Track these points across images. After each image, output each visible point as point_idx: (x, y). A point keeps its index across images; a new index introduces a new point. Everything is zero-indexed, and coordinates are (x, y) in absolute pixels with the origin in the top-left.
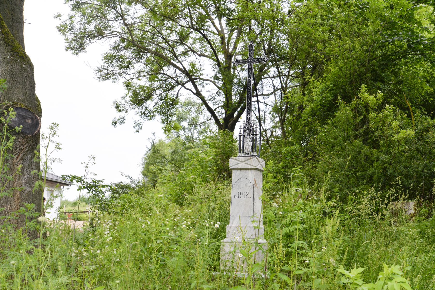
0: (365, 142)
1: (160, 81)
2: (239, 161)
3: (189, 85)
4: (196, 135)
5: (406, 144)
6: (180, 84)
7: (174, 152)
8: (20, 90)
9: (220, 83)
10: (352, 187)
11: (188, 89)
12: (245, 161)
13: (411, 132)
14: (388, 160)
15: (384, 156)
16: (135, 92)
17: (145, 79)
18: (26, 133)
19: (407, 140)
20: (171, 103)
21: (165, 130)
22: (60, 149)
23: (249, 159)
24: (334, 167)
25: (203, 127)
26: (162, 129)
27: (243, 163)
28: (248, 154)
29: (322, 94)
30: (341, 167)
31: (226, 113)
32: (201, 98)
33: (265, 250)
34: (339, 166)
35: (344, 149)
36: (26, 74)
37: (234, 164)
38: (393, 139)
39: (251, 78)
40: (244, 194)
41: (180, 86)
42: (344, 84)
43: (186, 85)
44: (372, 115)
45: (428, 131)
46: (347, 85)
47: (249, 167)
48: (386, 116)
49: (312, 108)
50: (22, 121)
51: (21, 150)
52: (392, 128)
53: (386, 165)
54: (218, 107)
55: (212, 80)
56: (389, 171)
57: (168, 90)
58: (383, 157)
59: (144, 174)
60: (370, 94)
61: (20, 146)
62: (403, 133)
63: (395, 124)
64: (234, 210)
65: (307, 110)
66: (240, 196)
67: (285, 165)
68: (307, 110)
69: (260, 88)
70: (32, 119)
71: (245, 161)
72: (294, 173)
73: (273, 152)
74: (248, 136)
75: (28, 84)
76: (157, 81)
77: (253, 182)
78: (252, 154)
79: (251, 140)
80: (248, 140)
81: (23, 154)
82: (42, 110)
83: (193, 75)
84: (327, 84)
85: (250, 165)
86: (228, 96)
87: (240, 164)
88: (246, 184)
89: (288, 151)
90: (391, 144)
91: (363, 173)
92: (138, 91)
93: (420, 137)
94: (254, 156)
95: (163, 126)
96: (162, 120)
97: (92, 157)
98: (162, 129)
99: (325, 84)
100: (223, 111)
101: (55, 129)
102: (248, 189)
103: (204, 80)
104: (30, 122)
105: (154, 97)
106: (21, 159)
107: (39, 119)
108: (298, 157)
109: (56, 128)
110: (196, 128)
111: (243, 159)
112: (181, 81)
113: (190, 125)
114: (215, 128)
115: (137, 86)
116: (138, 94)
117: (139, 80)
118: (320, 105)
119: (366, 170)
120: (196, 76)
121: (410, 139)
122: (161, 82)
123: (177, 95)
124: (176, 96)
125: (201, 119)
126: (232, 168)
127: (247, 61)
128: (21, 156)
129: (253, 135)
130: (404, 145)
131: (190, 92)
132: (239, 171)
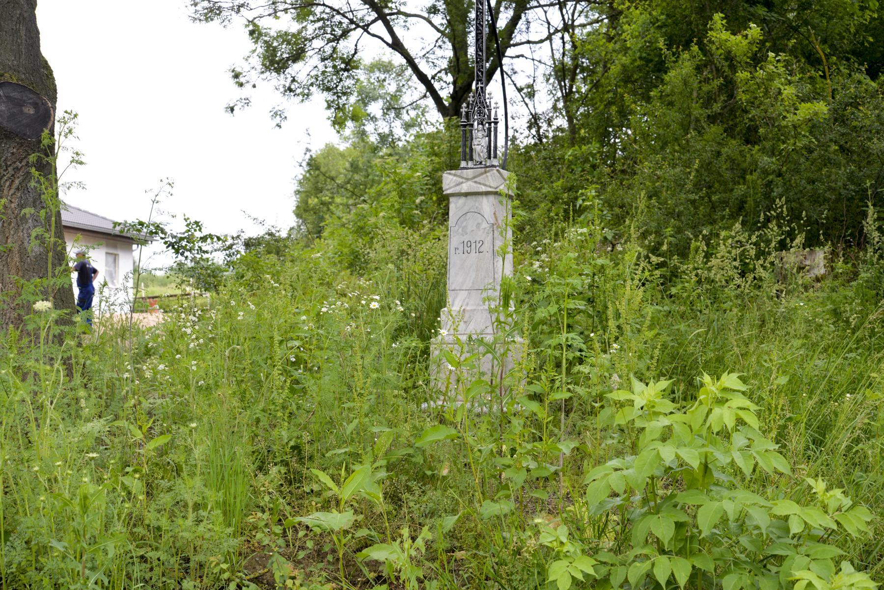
0: (730, 131)
1: (319, 20)
2: (462, 178)
3: (379, 28)
4: (399, 131)
5: (811, 133)
6: (358, 26)
7: (355, 167)
8: (9, 46)
9: (439, 20)
10: (703, 225)
11: (374, 35)
12: (474, 178)
13: (821, 108)
14: (773, 167)
15: (766, 158)
16: (268, 45)
17: (289, 16)
18: (25, 134)
19: (813, 125)
20: (343, 66)
21: (334, 123)
22: (81, 163)
23: (482, 174)
24: (665, 184)
25: (413, 113)
26: (329, 119)
27: (470, 183)
28: (481, 163)
29: (642, 35)
30: (680, 184)
31: (454, 83)
32: (402, 55)
33: (498, 354)
34: (675, 181)
35: (685, 149)
36: (18, 12)
37: (452, 185)
38: (784, 123)
39: (482, 4)
40: (473, 245)
41: (360, 30)
42: (687, 12)
43: (373, 29)
44: (742, 75)
45: (855, 105)
46: (694, 15)
47: (483, 189)
48: (771, 78)
49: (623, 66)
50: (15, 110)
51: (17, 169)
52: (782, 100)
53: (770, 177)
54: (440, 72)
55: (426, 15)
56: (775, 190)
57: (337, 39)
58: (766, 161)
59: (298, 215)
60: (734, 34)
61: (15, 162)
62: (805, 110)
63: (789, 91)
64: (454, 279)
65: (615, 69)
66: (466, 248)
67: (569, 185)
68: (615, 69)
69: (524, 27)
70: (35, 105)
71: (474, 178)
72: (584, 200)
73: (545, 159)
74: (480, 126)
75: (23, 33)
76: (314, 22)
77: (492, 221)
79: (486, 134)
80: (480, 134)
81: (21, 178)
82: (58, 88)
83: (386, 7)
84: (654, 13)
85: (485, 185)
86: (459, 47)
87: (464, 185)
89: (575, 156)
90: (782, 135)
91: (724, 195)
92: (275, 44)
93: (838, 117)
94: (493, 166)
95: (331, 113)
96: (327, 102)
97: (167, 181)
98: (329, 119)
99: (650, 14)
100: (450, 78)
101: (70, 124)
102: (483, 234)
103: (407, 15)
104: (32, 111)
105: (309, 53)
106: (18, 189)
107: (50, 105)
108: (594, 167)
109: (72, 122)
110: (398, 116)
111: (469, 173)
112: (362, 20)
113: (387, 109)
114: (434, 116)
115: (273, 33)
116: (275, 48)
117: (277, 18)
118: (641, 58)
119: (732, 190)
120: (391, 8)
121: (820, 122)
122: (320, 24)
123: (356, 50)
124: (353, 52)
125: (407, 99)
126: (448, 192)
128: (17, 182)
129: (490, 124)
130: (807, 134)
131: (380, 41)
132: (462, 200)
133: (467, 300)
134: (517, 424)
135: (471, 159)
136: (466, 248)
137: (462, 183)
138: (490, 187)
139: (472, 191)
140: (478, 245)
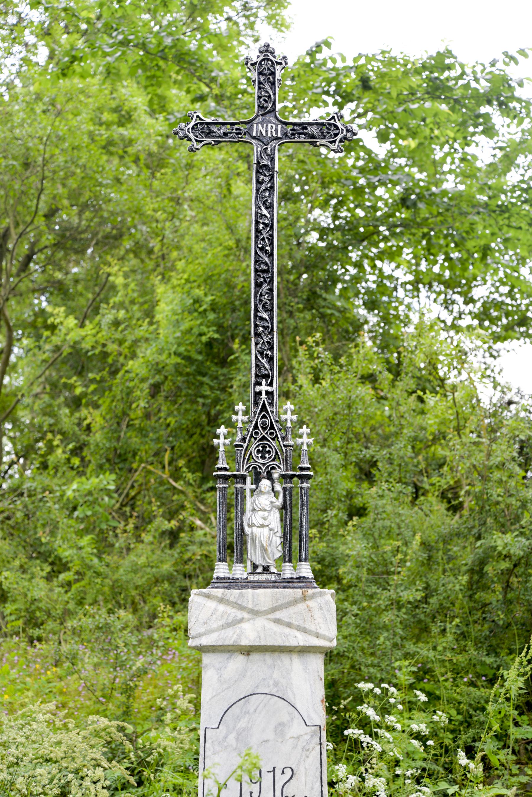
2: (241, 608)
12: (274, 610)
23: (295, 602)
27: (261, 622)
39: (270, 207)
40: (267, 779)
71: (274, 610)
78: (288, 571)
85: (305, 631)
87: (245, 626)
126: (205, 641)
127: (248, 133)
132: (239, 660)
134: (264, 395)
137: (241, 620)
139: (270, 642)
140: (281, 780)
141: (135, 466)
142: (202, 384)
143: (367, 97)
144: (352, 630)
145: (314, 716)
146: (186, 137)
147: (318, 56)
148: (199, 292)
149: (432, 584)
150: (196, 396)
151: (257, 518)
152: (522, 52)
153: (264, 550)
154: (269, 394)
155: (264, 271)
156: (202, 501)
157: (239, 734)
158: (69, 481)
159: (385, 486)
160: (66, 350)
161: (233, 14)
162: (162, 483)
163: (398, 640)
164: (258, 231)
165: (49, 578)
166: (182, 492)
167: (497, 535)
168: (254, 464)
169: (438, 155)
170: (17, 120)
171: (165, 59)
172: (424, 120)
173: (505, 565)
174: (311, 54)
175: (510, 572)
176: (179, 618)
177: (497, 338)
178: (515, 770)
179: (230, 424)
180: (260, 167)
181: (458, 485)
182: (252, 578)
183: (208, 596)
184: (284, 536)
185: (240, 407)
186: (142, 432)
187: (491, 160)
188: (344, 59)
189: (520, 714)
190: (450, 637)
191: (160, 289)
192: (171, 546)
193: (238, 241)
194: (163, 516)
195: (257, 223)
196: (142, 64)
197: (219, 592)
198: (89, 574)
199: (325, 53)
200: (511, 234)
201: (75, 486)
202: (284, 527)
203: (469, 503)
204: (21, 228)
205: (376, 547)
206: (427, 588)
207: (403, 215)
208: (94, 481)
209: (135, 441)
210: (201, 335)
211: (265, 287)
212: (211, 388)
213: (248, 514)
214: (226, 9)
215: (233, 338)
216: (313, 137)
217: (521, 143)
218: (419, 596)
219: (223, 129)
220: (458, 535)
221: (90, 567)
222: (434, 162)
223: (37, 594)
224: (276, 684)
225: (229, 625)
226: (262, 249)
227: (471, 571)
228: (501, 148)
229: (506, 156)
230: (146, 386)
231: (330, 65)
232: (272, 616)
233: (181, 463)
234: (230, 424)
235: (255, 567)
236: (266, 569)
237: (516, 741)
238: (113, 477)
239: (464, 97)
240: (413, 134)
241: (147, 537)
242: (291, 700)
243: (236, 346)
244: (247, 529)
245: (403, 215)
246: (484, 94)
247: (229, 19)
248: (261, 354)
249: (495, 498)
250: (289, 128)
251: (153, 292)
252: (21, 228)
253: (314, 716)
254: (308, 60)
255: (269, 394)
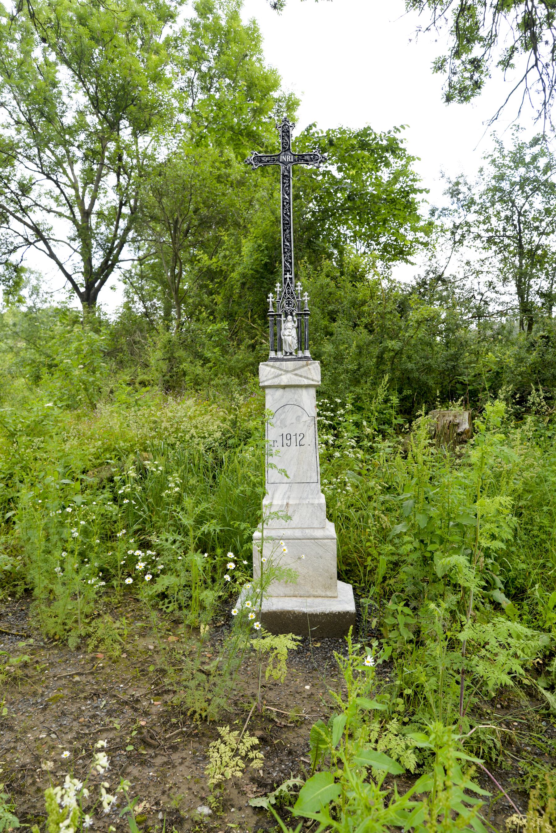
2: (281, 370)
3: (41, 244)
12: (294, 370)
23: (303, 366)
27: (289, 375)
40: (293, 438)
47: (306, 382)
55: (68, 241)
66: (285, 441)
71: (294, 370)
78: (300, 354)
85: (308, 378)
86: (88, 261)
87: (283, 377)
88: (298, 418)
111: (290, 365)
126: (266, 384)
127: (278, 160)
132: (280, 392)
133: (288, 493)
135: (281, 350)
136: (285, 441)
137: (281, 375)
138: (313, 380)
140: (299, 439)
141: (236, 318)
142: (263, 282)
143: (332, 149)
144: (328, 382)
145: (312, 413)
146: (251, 163)
147: (311, 131)
148: (260, 242)
149: (361, 363)
150: (261, 287)
151: (287, 332)
152: (402, 126)
153: (290, 345)
154: (290, 279)
155: (287, 224)
156: (265, 332)
157: (281, 421)
158: (209, 326)
159: (340, 322)
160: (205, 269)
161: (272, 115)
162: (247, 325)
163: (347, 385)
164: (284, 206)
165: (202, 366)
166: (256, 329)
167: (388, 341)
168: (284, 309)
169: (365, 178)
170: (178, 167)
171: (242, 135)
172: (358, 160)
173: (392, 354)
174: (308, 130)
175: (394, 357)
176: (256, 379)
177: (389, 260)
178: (395, 436)
179: (275, 293)
180: (284, 176)
181: (373, 322)
182: (285, 357)
183: (267, 365)
184: (298, 340)
185: (278, 285)
186: (239, 304)
187: (388, 179)
188: (322, 132)
189: (397, 414)
190: (369, 384)
191: (243, 241)
192: (253, 351)
193: (276, 218)
194: (249, 338)
195: (283, 202)
196: (231, 139)
197: (271, 363)
198: (219, 363)
199: (314, 130)
200: (396, 212)
201: (211, 328)
202: (298, 335)
203: (377, 330)
204: (183, 217)
205: (337, 348)
206: (359, 364)
207: (349, 204)
208: (219, 325)
209: (236, 308)
210: (262, 260)
211: (288, 231)
212: (267, 284)
213: (283, 330)
214: (269, 113)
215: (276, 262)
216: (307, 161)
217: (401, 171)
218: (356, 368)
219: (267, 159)
220: (372, 342)
221: (219, 361)
222: (363, 181)
223: (198, 372)
224: (296, 400)
225: (276, 377)
226: (286, 214)
227: (378, 357)
228: (392, 173)
229: (395, 177)
230: (239, 283)
231: (316, 135)
232: (294, 373)
233: (255, 316)
234: (275, 293)
235: (286, 353)
236: (291, 354)
237: (395, 425)
238: (227, 323)
239: (376, 149)
240: (354, 167)
241: (242, 348)
242: (302, 406)
243: (277, 265)
244: (283, 337)
245: (349, 204)
246: (385, 147)
247: (270, 118)
248: (287, 261)
249: (388, 326)
250: (296, 157)
251: (241, 242)
252: (183, 217)
253: (312, 413)
254: (306, 133)
255: (290, 279)
